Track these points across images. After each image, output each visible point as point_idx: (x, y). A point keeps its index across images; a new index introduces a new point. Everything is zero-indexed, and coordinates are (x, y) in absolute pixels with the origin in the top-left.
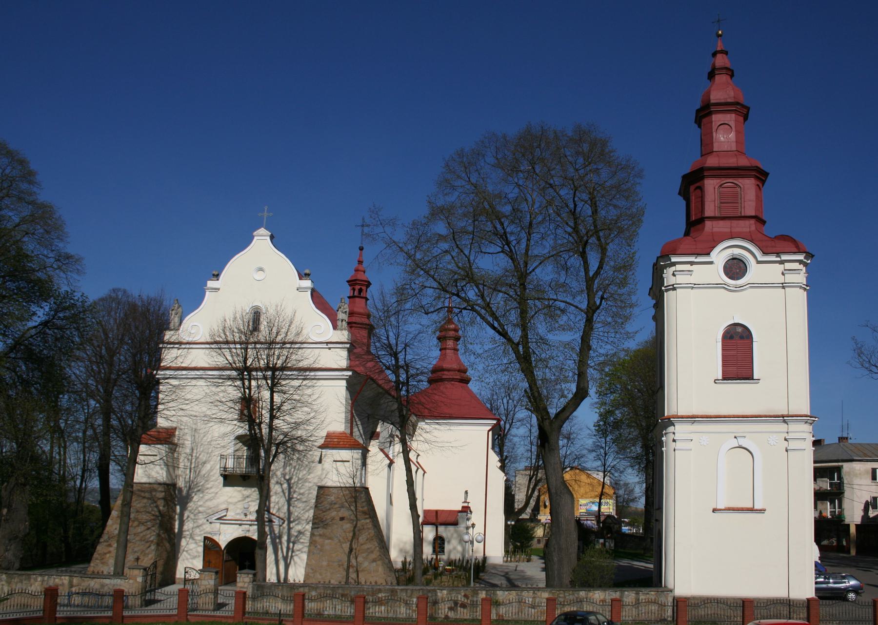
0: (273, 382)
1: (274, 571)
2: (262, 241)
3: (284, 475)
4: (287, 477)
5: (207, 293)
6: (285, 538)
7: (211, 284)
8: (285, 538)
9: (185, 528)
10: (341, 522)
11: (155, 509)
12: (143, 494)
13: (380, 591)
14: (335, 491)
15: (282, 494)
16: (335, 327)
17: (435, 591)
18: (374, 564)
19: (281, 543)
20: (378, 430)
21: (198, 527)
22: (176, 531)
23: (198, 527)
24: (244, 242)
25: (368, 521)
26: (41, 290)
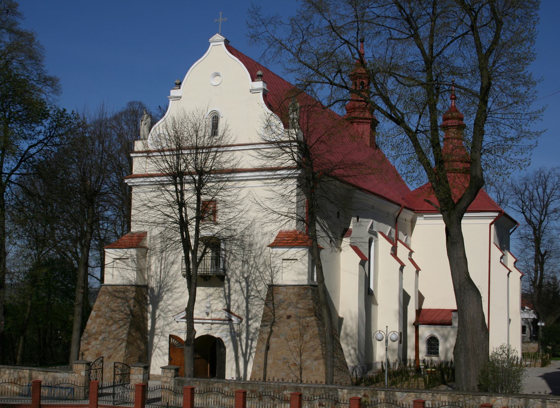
0: (199, 185)
1: (234, 367)
2: (217, 48)
3: (242, 273)
4: (246, 275)
5: (171, 102)
6: (244, 336)
7: (174, 93)
8: (244, 336)
9: (157, 325)
10: (288, 320)
11: (127, 309)
12: (117, 294)
13: (285, 388)
14: (284, 289)
15: (241, 292)
16: (286, 126)
17: (336, 389)
18: (316, 363)
19: (240, 340)
20: (351, 227)
21: (168, 324)
22: (149, 328)
23: (168, 324)
24: (201, 49)
25: (313, 318)
26: (35, 112)
